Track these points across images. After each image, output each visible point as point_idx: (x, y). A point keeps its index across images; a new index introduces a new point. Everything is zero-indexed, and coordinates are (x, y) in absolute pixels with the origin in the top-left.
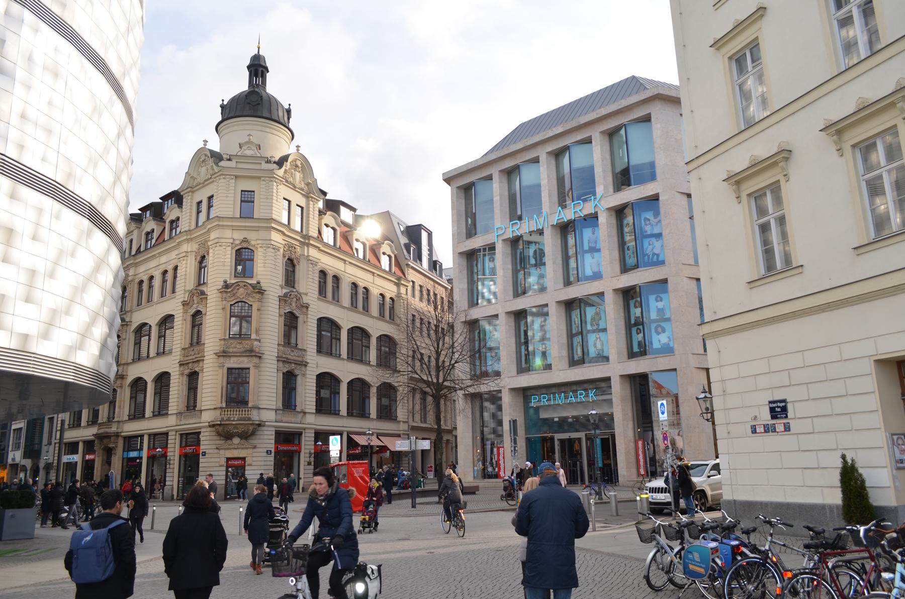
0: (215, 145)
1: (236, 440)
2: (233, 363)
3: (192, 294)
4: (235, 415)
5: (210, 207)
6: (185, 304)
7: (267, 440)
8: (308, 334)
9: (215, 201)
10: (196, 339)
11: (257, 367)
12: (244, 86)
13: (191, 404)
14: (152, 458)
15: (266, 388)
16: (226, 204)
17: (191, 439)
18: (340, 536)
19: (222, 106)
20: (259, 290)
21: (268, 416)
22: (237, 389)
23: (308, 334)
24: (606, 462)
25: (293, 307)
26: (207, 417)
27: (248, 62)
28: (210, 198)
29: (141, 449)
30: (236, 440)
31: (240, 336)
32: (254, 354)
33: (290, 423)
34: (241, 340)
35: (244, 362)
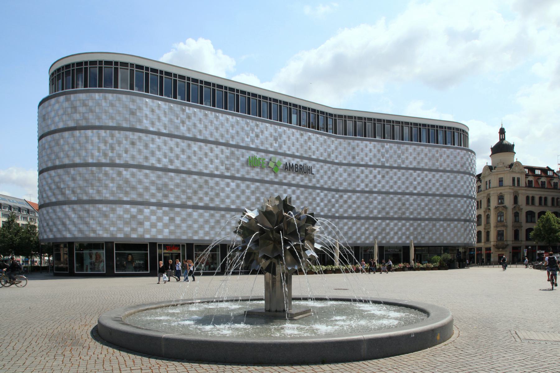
0: (490, 164)
1: (501, 250)
2: (499, 229)
3: (486, 209)
4: (500, 243)
5: (490, 183)
6: (484, 212)
7: (510, 249)
8: (523, 217)
9: (491, 182)
10: (488, 223)
11: (506, 229)
12: (497, 140)
13: (488, 239)
14: (477, 254)
15: (509, 235)
16: (495, 182)
17: (488, 249)
18: (51, 111)
19: (492, 149)
20: (505, 207)
21: (509, 243)
22: (500, 235)
23: (523, 217)
24: (239, 260)
25: (517, 210)
26: (492, 243)
27: (499, 131)
28: (490, 181)
29: (121, 88)
30: (501, 250)
31: (501, 221)
32: (506, 226)
33: (517, 244)
34: (500, 222)
35: (502, 229)
